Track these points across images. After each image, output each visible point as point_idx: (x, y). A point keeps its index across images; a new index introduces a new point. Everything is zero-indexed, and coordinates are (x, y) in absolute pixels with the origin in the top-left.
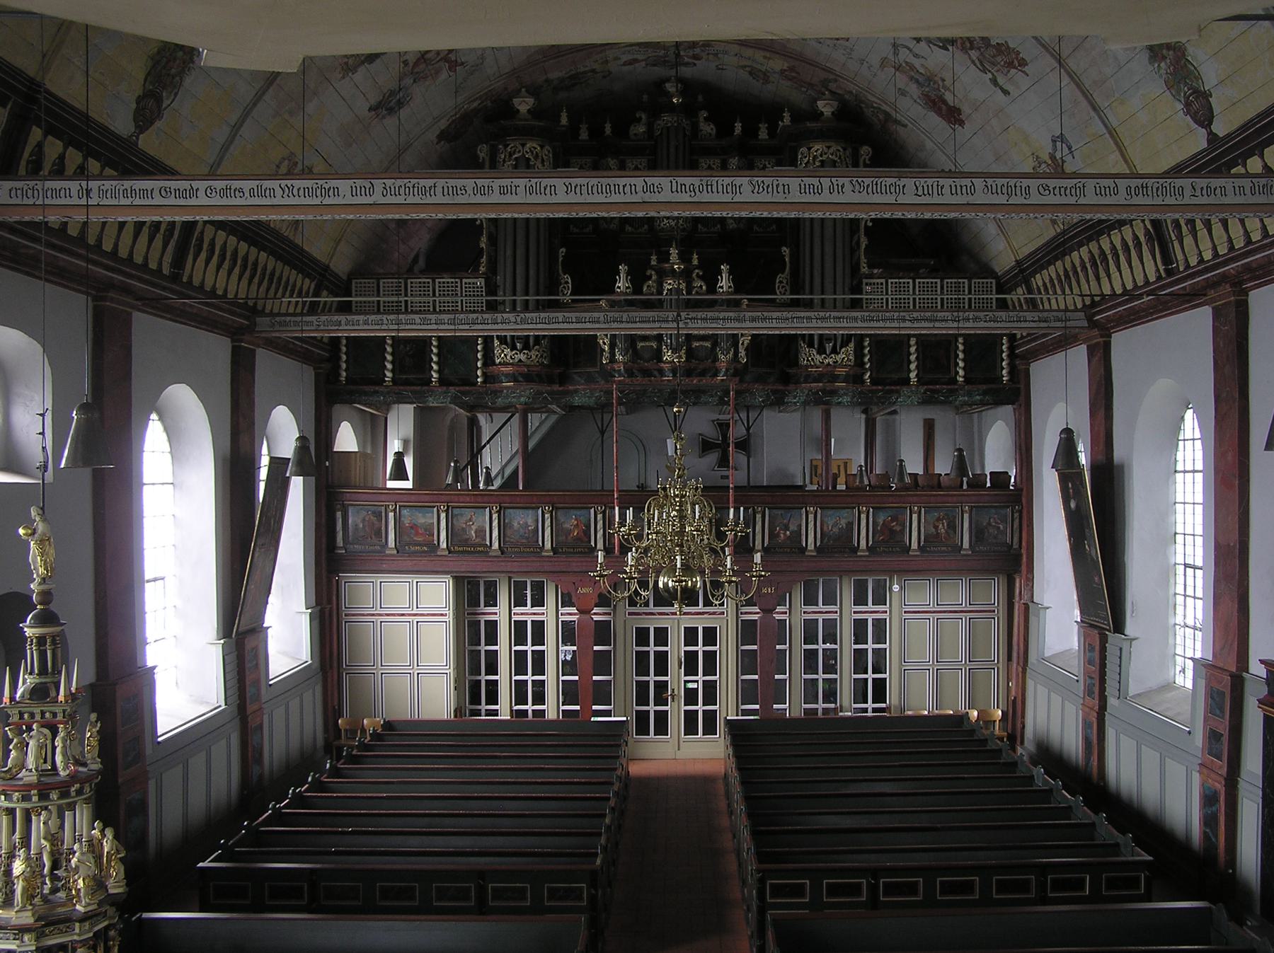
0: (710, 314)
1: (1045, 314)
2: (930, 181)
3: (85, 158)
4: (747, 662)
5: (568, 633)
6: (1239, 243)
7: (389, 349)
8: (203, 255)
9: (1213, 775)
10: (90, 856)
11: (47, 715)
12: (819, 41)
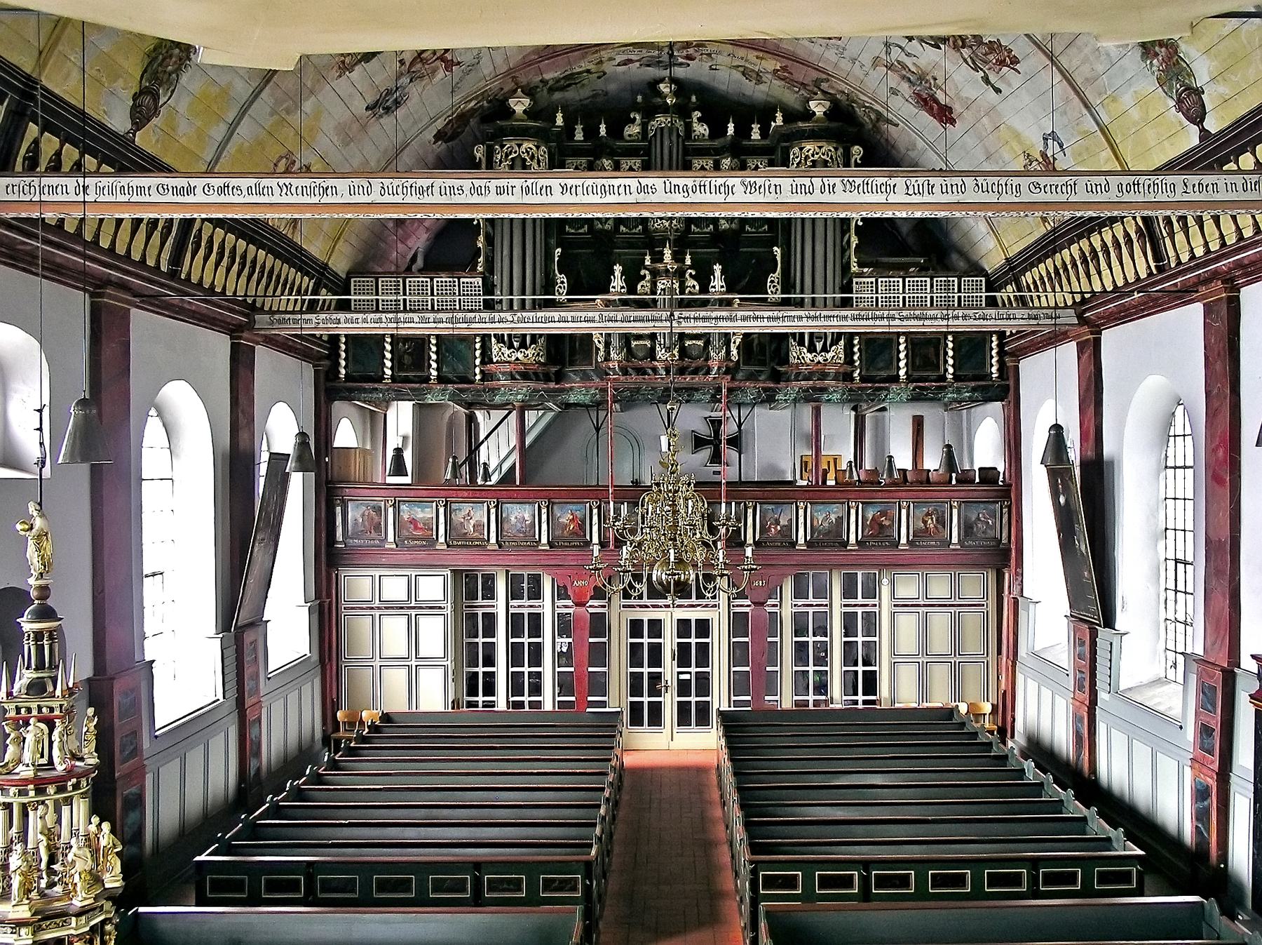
0: (703, 314)
1: (1035, 312)
2: (921, 180)
3: (82, 155)
4: (738, 654)
5: (564, 626)
6: (1231, 240)
7: (388, 347)
8: (201, 253)
9: (1205, 770)
10: (87, 850)
11: (44, 710)
12: (811, 41)
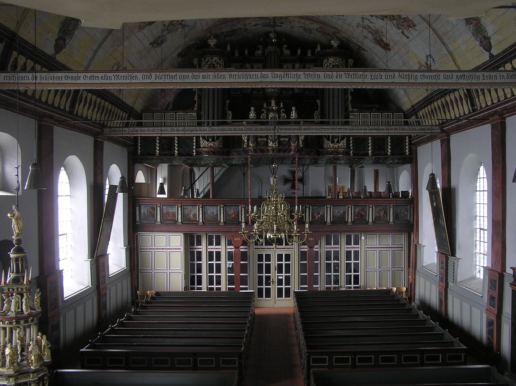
10: (37, 346)
11: (19, 289)
